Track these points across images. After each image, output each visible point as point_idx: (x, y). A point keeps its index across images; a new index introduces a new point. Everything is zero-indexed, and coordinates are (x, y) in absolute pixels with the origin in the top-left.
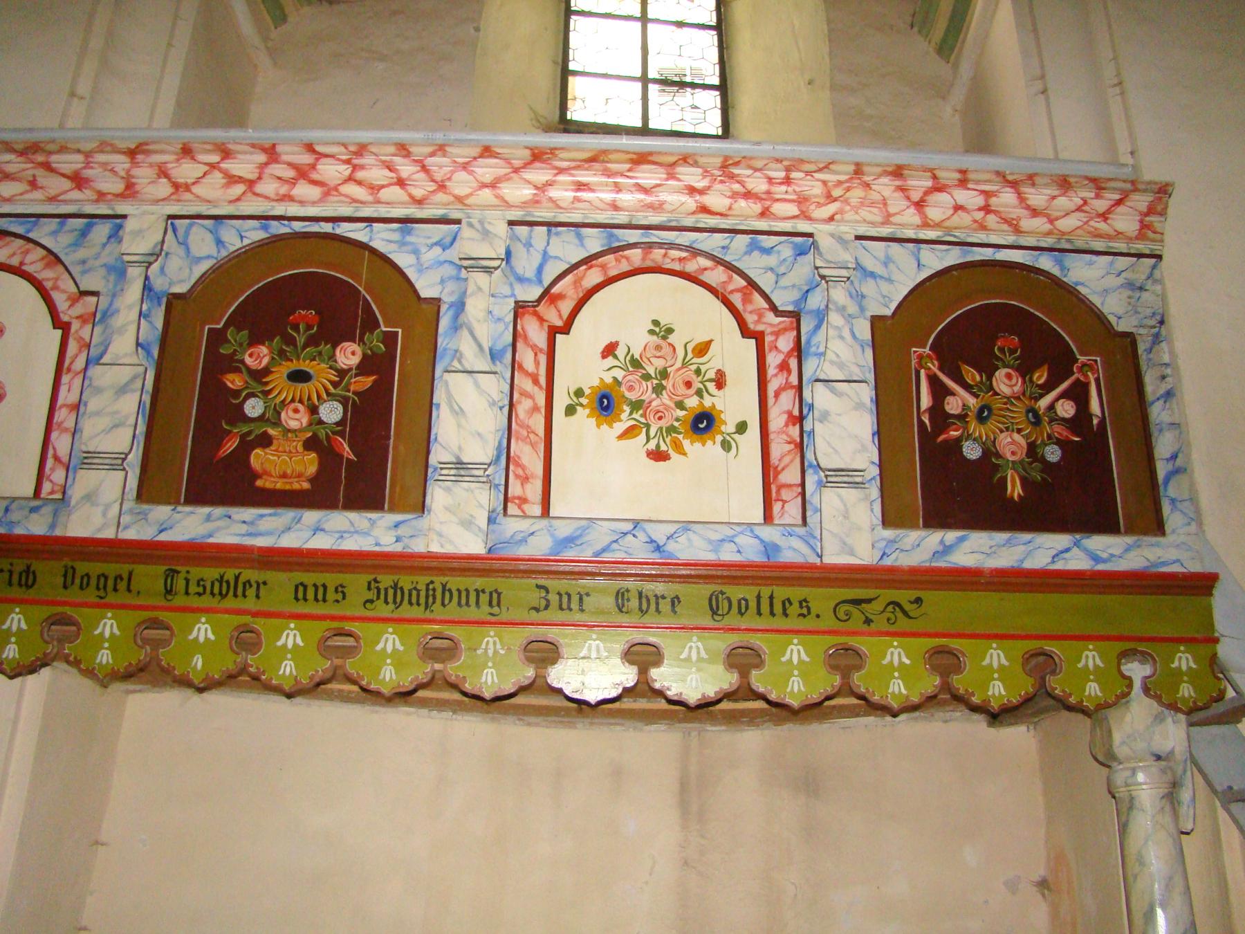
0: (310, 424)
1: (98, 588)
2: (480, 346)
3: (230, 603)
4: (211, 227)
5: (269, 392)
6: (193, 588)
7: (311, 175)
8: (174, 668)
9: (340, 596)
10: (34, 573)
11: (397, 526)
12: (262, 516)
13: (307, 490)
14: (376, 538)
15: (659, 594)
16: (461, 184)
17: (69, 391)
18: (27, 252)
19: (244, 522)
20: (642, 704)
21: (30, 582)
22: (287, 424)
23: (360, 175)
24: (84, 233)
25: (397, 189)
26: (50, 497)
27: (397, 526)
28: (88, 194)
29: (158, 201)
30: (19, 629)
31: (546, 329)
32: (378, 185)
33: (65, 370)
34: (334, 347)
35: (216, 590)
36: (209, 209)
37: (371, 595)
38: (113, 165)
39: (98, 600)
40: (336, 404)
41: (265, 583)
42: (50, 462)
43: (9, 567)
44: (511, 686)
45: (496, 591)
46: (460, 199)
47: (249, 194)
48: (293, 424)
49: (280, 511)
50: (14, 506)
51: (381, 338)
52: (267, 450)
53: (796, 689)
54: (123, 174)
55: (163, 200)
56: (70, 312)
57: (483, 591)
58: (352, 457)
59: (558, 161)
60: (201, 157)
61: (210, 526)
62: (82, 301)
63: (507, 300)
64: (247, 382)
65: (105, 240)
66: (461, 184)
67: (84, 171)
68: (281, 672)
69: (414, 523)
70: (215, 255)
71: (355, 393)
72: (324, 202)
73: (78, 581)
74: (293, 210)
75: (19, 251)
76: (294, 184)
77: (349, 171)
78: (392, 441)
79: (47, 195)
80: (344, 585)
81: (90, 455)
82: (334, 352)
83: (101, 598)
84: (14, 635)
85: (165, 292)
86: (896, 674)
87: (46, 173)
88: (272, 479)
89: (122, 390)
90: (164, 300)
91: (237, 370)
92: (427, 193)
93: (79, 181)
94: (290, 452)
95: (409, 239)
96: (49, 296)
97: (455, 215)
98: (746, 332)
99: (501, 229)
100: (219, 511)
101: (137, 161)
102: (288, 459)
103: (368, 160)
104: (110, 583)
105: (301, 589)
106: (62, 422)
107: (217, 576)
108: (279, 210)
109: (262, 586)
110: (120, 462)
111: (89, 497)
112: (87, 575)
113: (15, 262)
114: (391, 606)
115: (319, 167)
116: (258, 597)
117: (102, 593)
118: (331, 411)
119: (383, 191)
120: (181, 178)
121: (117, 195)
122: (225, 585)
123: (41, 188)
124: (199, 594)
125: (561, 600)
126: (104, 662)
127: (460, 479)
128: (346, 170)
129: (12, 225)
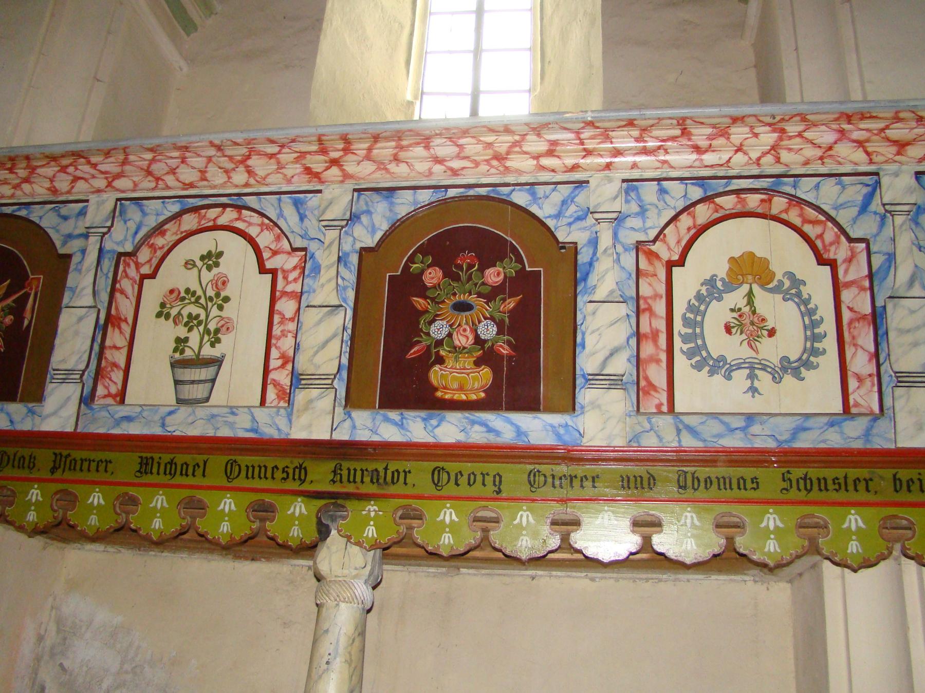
3: (179, 480)
8: (77, 526)
9: (755, 485)
10: (305, 469)
13: (483, 399)
37: (785, 485)
41: (871, 480)
43: (918, 477)
44: (707, 555)
53: (370, 535)
57: (488, 474)
68: (153, 527)
73: (702, 484)
84: (772, 532)
98: (821, 261)
102: (467, 376)
105: (185, 467)
110: (329, 382)
112: (397, 471)
114: (804, 492)
122: (808, 481)
126: (296, 535)
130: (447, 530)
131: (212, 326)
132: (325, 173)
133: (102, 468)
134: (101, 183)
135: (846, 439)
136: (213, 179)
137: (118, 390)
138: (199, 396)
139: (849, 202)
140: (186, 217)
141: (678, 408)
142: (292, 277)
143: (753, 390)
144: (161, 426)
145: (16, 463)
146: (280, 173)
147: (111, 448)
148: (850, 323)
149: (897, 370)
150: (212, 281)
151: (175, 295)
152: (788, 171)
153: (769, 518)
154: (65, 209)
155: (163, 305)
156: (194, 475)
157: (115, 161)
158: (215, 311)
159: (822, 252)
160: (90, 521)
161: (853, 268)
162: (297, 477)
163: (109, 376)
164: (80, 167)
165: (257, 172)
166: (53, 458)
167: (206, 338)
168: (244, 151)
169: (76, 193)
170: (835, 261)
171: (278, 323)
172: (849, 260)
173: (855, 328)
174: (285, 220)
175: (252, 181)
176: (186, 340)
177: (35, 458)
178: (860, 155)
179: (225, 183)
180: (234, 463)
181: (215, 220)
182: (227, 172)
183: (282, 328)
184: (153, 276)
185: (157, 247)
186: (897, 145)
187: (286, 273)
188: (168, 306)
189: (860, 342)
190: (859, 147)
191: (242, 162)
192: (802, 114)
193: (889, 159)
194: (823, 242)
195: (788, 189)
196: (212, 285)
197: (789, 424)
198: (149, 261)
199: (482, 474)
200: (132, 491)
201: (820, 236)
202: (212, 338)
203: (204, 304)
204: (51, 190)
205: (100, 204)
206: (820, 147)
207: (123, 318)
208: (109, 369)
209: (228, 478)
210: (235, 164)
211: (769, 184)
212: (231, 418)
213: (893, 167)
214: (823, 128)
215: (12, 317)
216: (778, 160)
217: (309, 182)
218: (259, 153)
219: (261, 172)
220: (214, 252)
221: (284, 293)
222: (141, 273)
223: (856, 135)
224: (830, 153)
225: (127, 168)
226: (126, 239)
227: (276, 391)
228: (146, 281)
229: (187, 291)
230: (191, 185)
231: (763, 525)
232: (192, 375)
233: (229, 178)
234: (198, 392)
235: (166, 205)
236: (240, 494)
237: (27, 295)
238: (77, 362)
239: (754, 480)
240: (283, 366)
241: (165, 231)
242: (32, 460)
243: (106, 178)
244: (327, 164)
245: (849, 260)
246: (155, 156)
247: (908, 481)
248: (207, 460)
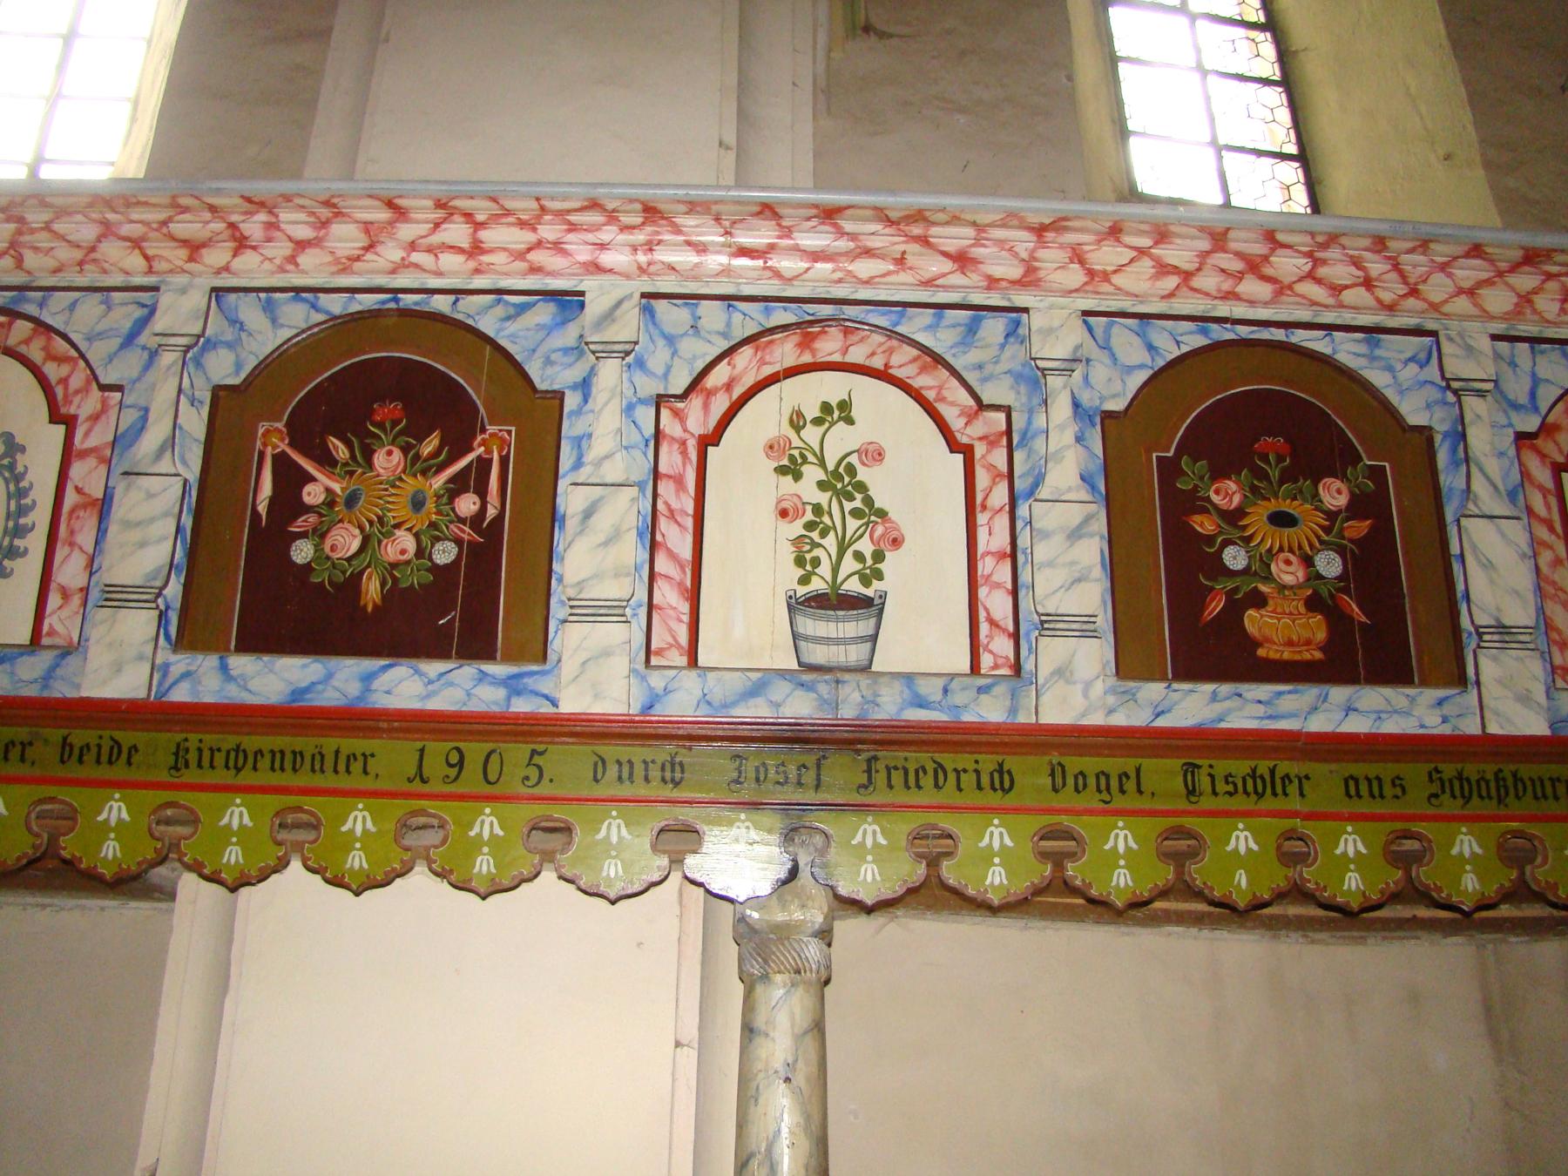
0: (1308, 580)
1: (1099, 790)
2: (1495, 487)
3: (1269, 803)
4: (1136, 328)
5: (1251, 537)
6: (1221, 787)
7: (1263, 269)
9: (1398, 791)
10: (1009, 772)
11: (1440, 703)
12: (1280, 693)
13: (1320, 661)
14: (1419, 719)
15: (1555, 776)
16: (1438, 287)
17: (990, 534)
18: (891, 351)
19: (1260, 702)
20: (1293, 910)
21: (1007, 784)
22: (1280, 578)
23: (1322, 271)
24: (972, 329)
25: (1362, 290)
26: (993, 673)
27: (1440, 703)
28: (974, 279)
29: (1071, 292)
30: (120, 820)
31: (1549, 466)
32: (1340, 285)
33: (978, 509)
34: (1316, 484)
35: (1250, 788)
36: (1134, 305)
38: (1012, 244)
39: (1102, 805)
40: (1333, 555)
41: (1307, 777)
42: (984, 628)
45: (1081, 773)
46: (1434, 307)
47: (1185, 289)
48: (1288, 579)
49: (1300, 687)
50: (955, 685)
51: (1367, 474)
52: (1263, 612)
54: (1024, 255)
55: (1076, 290)
56: (969, 431)
58: (1363, 619)
59: (1551, 265)
60: (1128, 239)
61: (1218, 708)
62: (981, 418)
63: (1505, 430)
64: (1220, 526)
65: (1001, 340)
66: (1438, 287)
67: (973, 249)
68: (1345, 888)
69: (1458, 699)
70: (1150, 364)
71: (1351, 541)
72: (1275, 303)
73: (1070, 781)
74: (1240, 311)
75: (879, 350)
76: (1241, 279)
77: (1309, 266)
78: (1407, 600)
79: (918, 277)
80: (1402, 776)
81: (1050, 618)
82: (1317, 490)
83: (1106, 802)
84: (1467, 862)
85: (1097, 408)
87: (924, 250)
88: (1275, 647)
89: (1075, 535)
90: (1098, 420)
91: (1204, 511)
92: (1395, 297)
93: (962, 260)
94: (1291, 614)
95: (1378, 352)
96: (935, 409)
97: (1431, 325)
99: (1485, 344)
100: (1225, 688)
101: (1046, 239)
103: (1333, 253)
104: (1114, 783)
105: (1351, 783)
106: (990, 576)
107: (1455, 774)
108: (1223, 310)
109: (1304, 781)
111: (1061, 673)
113: (877, 363)
114: (1460, 801)
115: (1272, 259)
116: (1302, 794)
117: (1106, 797)
118: (1328, 563)
119: (1345, 293)
120: (1098, 264)
121: (1013, 283)
122: (1259, 782)
123: (911, 268)
124: (1230, 794)
125: (620, 771)
126: (1122, 884)
127: (1506, 645)
128: (1304, 264)
129: (870, 315)
130: (358, 845)
135: (17, 682)
139: (111, 329)
141: (703, 660)
147: (374, 732)
148: (72, 512)
149: (108, 583)
152: (31, 281)
153: (1346, 840)
156: (348, 771)
159: (60, 404)
161: (98, 428)
162: (231, 763)
170: (75, 418)
172: (95, 418)
173: (78, 517)
178: (135, 261)
186: (187, 247)
189: (80, 539)
190: (134, 248)
192: (39, 195)
193: (177, 267)
194: (66, 388)
195: (31, 309)
197: (736, 682)
199: (955, 770)
201: (64, 381)
206: (78, 246)
211: (7, 300)
213: (181, 280)
214: (79, 217)
216: (19, 261)
223: (126, 230)
224: (93, 255)
228: (710, 449)
231: (1338, 852)
236: (259, 798)
239: (1396, 781)
242: (1501, 783)
245: (95, 418)
247: (81, 749)
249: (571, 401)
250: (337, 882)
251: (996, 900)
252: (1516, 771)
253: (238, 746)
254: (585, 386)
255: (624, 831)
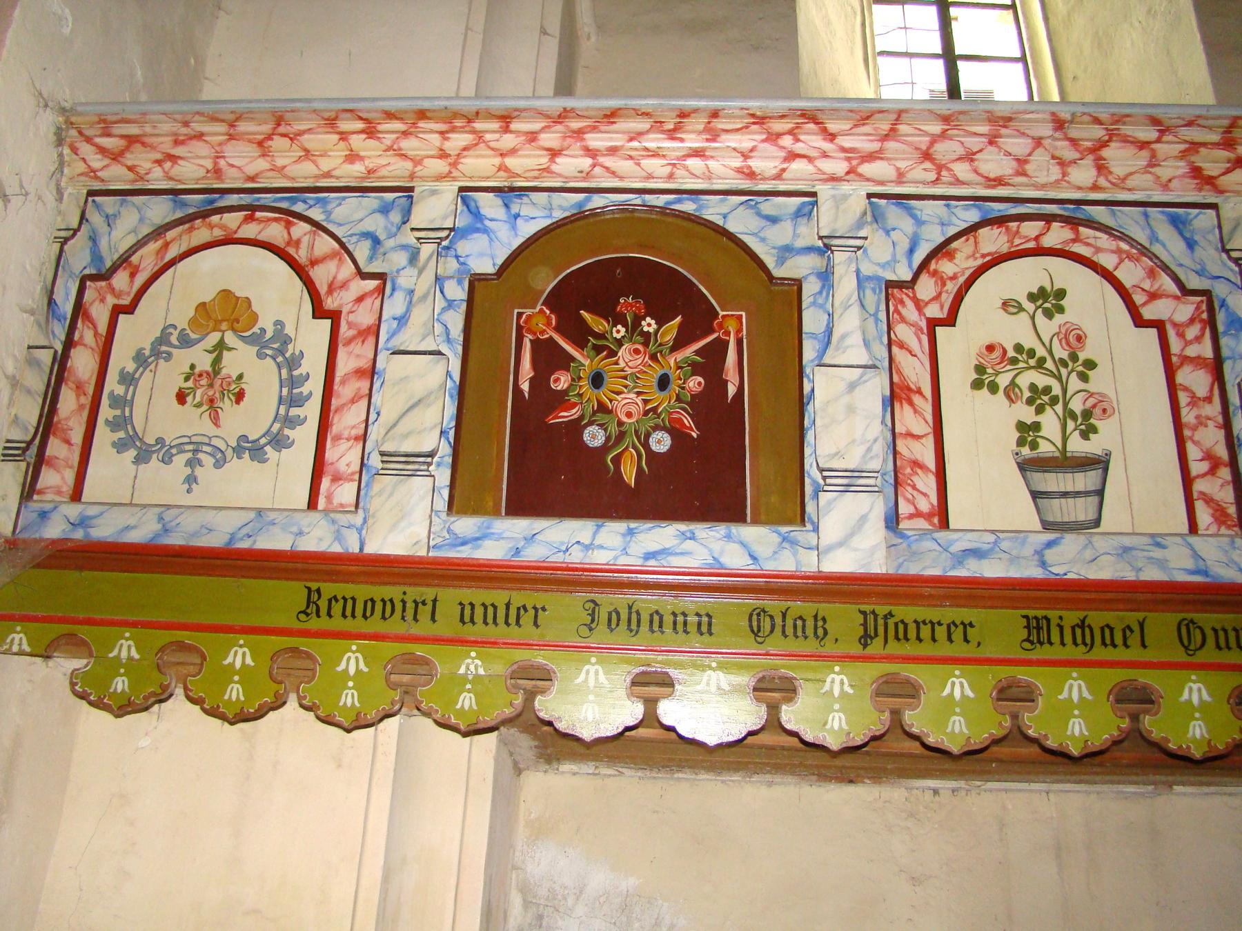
57: (940, 624)
68: (226, 697)
84: (237, 673)
86: (958, 710)
105: (1107, 631)
116: (536, 624)
122: (1087, 631)
126: (234, 698)
131: (1077, 405)
132: (1222, 178)
133: (958, 634)
134: (838, 166)
136: (1036, 174)
137: (932, 505)
138: (1081, 517)
140: (984, 232)
142: (1192, 332)
143: (191, 480)
144: (1038, 566)
145: (789, 630)
146: (1150, 173)
150: (1058, 334)
151: (997, 354)
154: (767, 203)
155: (980, 369)
157: (874, 132)
158: (1074, 383)
160: (113, 686)
163: (909, 481)
164: (802, 137)
165: (1112, 169)
166: (861, 619)
167: (1071, 425)
168: (1098, 132)
169: (155, 180)
171: (1188, 404)
174: (1164, 246)
175: (1102, 182)
176: (1036, 426)
177: (824, 619)
179: (1057, 181)
180: (1191, 625)
181: (1037, 238)
182: (1062, 163)
183: (1195, 412)
184: (950, 320)
185: (945, 277)
187: (1180, 329)
188: (990, 371)
191: (1093, 150)
196: (1060, 341)
198: (937, 297)
200: (1023, 674)
202: (1081, 425)
203: (1053, 369)
204: (743, 173)
205: (840, 200)
207: (913, 387)
208: (908, 470)
209: (1186, 648)
210: (1081, 153)
212: (1157, 553)
215: (700, 379)
217: (1200, 190)
218: (1126, 140)
219: (1118, 170)
220: (1049, 288)
221: (1185, 360)
222: (928, 315)
225: (891, 145)
226: (895, 260)
227: (1211, 511)
228: (122, 317)
229: (1019, 348)
230: (999, 181)
232: (1062, 485)
233: (1064, 174)
234: (1081, 510)
235: (954, 210)
237: (721, 346)
238: (864, 456)
240: (1212, 471)
241: (955, 250)
242: (820, 623)
243: (848, 159)
244: (1228, 165)
246: (947, 130)
248: (1144, 620)
249: (811, 288)
250: (213, 712)
251: (1197, 754)
252: (874, 610)
253: (1083, 621)
254: (826, 276)
255: (602, 677)
